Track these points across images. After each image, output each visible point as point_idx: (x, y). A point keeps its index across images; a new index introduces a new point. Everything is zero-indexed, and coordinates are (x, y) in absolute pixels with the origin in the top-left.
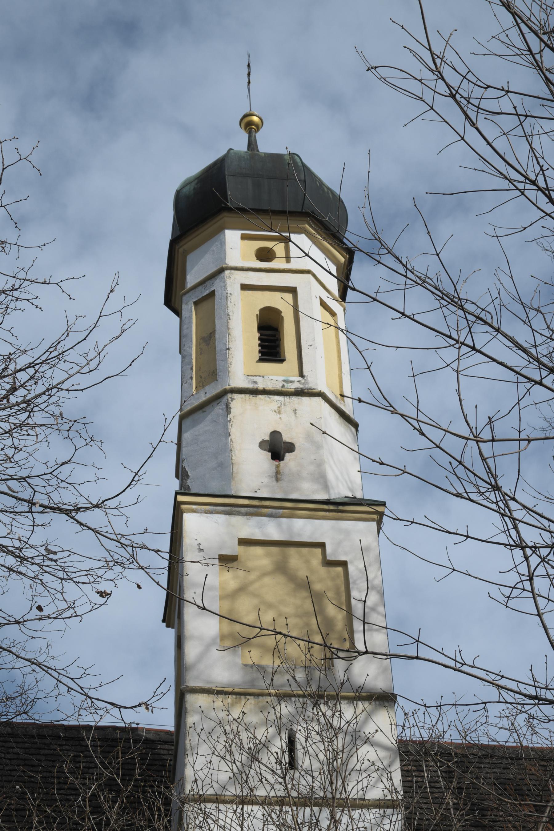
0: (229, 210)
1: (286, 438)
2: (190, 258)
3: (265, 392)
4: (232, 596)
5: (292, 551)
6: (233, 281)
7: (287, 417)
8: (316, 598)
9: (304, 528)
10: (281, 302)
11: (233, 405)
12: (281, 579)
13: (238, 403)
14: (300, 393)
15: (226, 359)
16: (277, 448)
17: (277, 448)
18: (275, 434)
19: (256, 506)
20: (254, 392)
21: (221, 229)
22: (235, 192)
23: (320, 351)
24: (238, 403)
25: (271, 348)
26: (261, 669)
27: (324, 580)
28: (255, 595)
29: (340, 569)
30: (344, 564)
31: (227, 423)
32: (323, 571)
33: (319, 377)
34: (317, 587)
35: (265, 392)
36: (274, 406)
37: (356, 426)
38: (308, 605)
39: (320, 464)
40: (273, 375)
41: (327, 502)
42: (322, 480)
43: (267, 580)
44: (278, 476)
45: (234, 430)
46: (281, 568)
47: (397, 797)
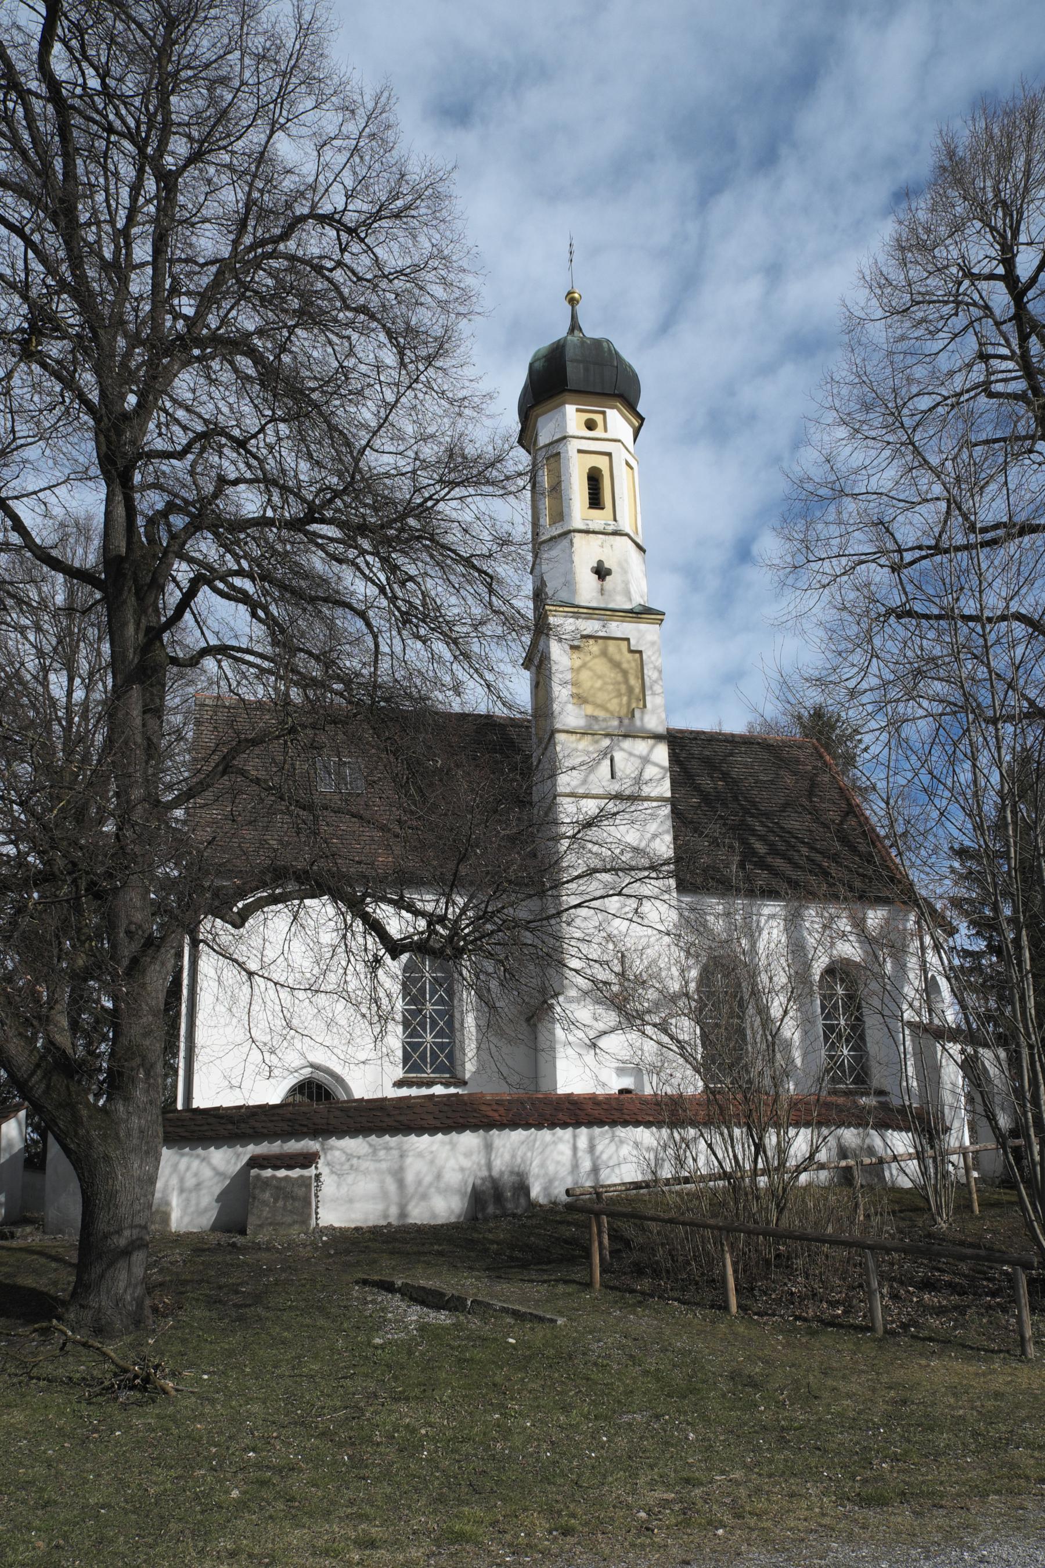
0: (570, 391)
1: (607, 565)
2: (541, 421)
3: (594, 532)
4: (576, 671)
5: (611, 642)
6: (573, 446)
7: (607, 550)
8: (625, 673)
9: (617, 628)
10: (602, 463)
11: (575, 541)
12: (603, 660)
13: (578, 538)
14: (615, 533)
15: (569, 507)
16: (601, 572)
17: (601, 572)
18: (600, 563)
19: (592, 613)
20: (587, 532)
21: (564, 403)
22: (574, 372)
23: (626, 502)
24: (578, 538)
25: (595, 501)
26: (595, 718)
27: (628, 661)
28: (590, 669)
29: (637, 655)
30: (640, 652)
31: (571, 554)
32: (629, 656)
33: (626, 523)
34: (625, 666)
35: (594, 532)
36: (599, 542)
37: (644, 551)
38: (620, 678)
39: (626, 583)
40: (599, 519)
41: (631, 611)
42: (628, 594)
43: (596, 660)
44: (602, 591)
45: (576, 558)
46: (604, 653)
47: (931, 1020)
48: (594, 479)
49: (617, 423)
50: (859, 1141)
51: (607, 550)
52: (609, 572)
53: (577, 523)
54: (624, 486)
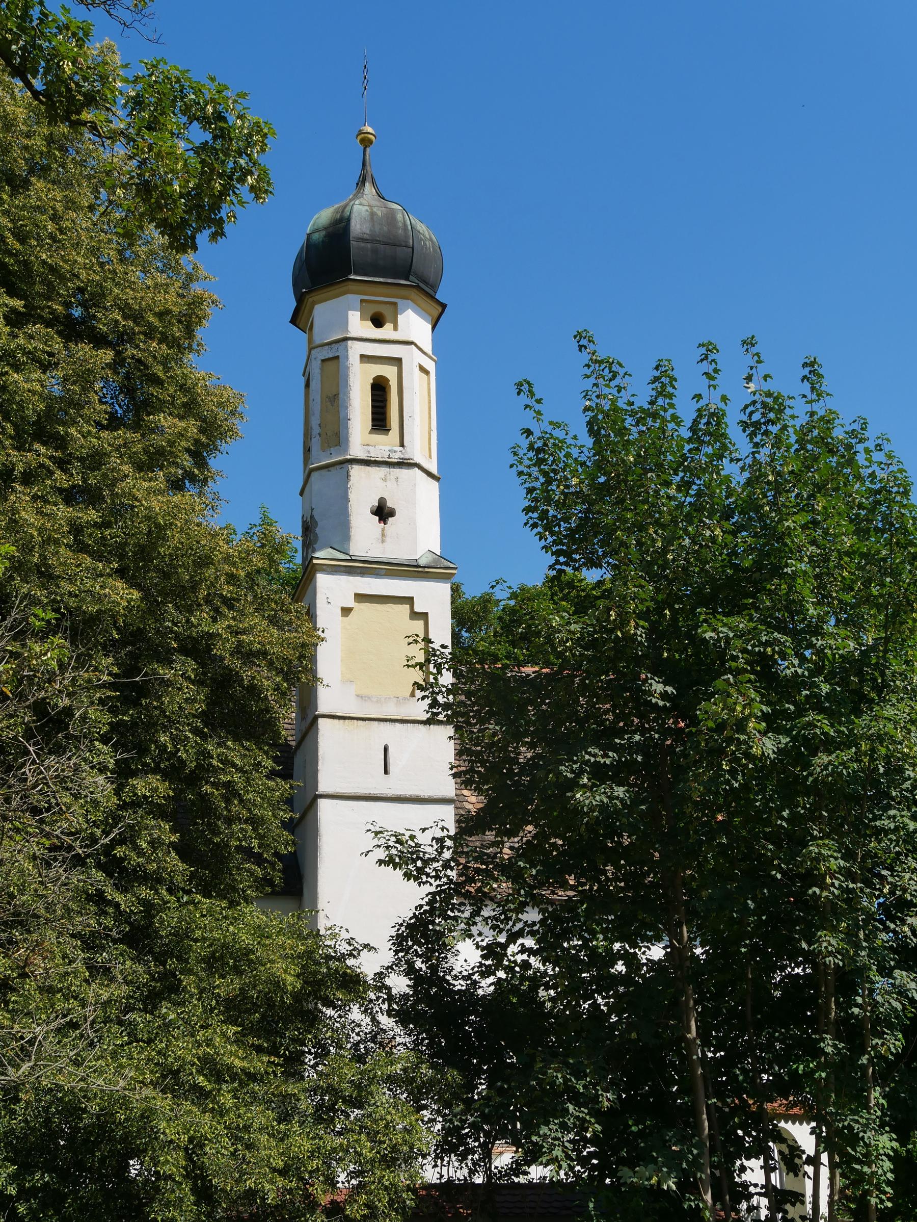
1: (390, 504)
2: (314, 303)
6: (355, 350)
7: (391, 484)
10: (389, 372)
13: (356, 471)
15: (347, 428)
16: (383, 512)
24: (356, 471)
25: (380, 422)
40: (383, 446)
45: (352, 496)
48: (379, 389)
49: (413, 324)
50: (457, 969)
51: (391, 484)
52: (392, 513)
53: (356, 450)
54: (419, 401)
